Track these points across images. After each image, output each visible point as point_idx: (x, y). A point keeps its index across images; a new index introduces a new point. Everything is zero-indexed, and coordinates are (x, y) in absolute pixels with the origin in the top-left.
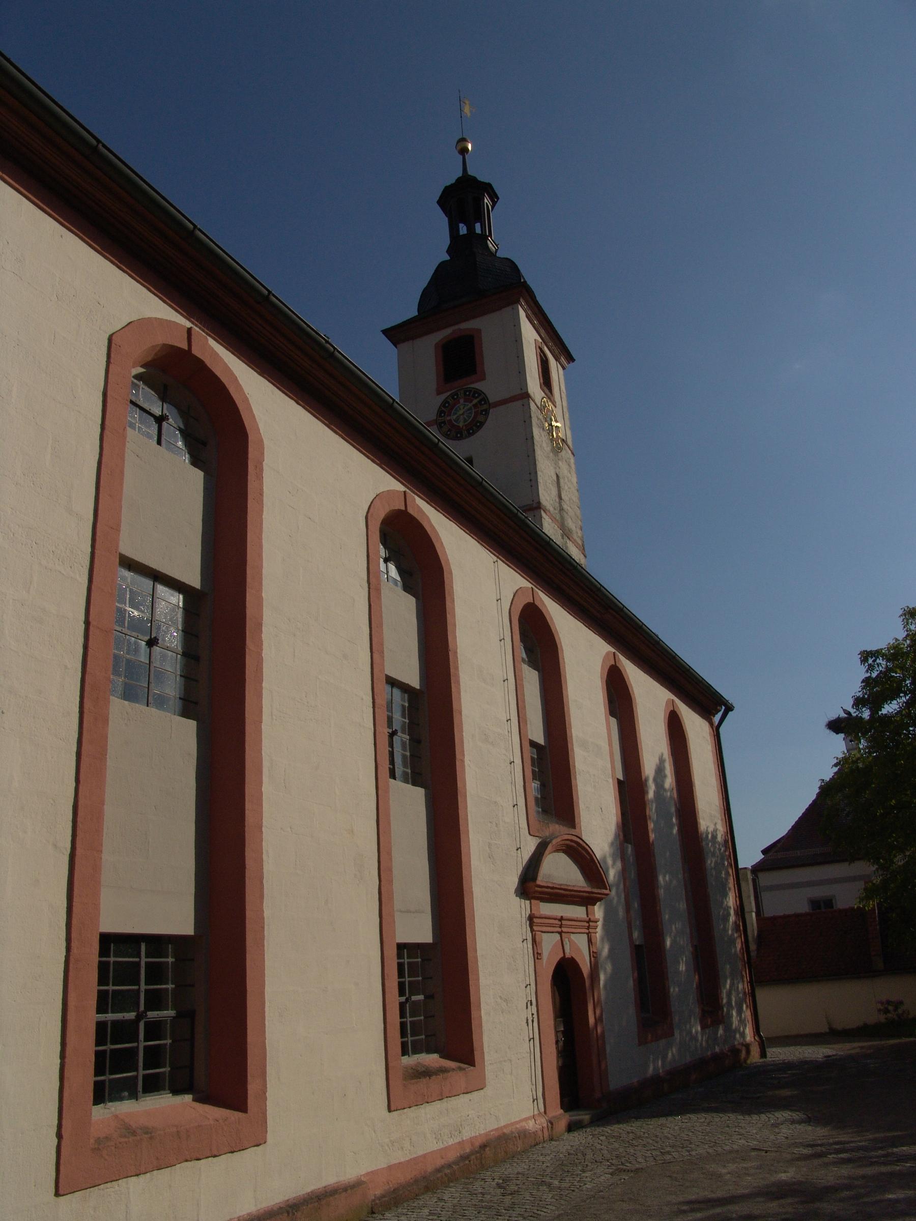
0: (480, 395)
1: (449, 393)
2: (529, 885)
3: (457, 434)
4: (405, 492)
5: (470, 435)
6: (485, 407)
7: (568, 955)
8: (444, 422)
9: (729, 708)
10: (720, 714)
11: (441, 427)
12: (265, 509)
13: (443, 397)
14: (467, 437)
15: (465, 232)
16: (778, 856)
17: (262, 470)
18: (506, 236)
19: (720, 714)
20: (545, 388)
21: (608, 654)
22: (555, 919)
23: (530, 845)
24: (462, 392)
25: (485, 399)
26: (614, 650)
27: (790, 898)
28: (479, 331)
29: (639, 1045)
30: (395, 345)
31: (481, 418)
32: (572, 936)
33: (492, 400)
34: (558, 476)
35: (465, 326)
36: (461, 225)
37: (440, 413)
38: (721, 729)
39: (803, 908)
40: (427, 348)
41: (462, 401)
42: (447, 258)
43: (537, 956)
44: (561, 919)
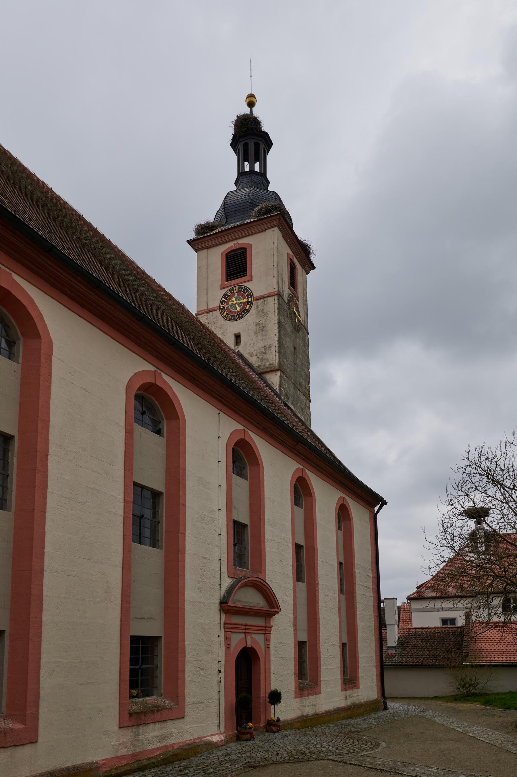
0: (248, 291)
1: (229, 288)
2: (225, 606)
3: (231, 317)
4: (155, 371)
5: (240, 318)
6: (251, 299)
7: (249, 645)
8: (224, 308)
9: (384, 503)
10: (378, 506)
11: (222, 312)
12: (52, 384)
13: (224, 291)
14: (238, 320)
15: (248, 170)
16: (422, 595)
17: (51, 360)
18: (281, 172)
19: (378, 506)
20: (292, 289)
21: (297, 469)
22: (242, 625)
23: (227, 582)
24: (237, 288)
25: (250, 295)
26: (301, 467)
27: (427, 619)
28: (251, 246)
29: (295, 698)
30: (196, 251)
31: (247, 307)
32: (253, 636)
33: (256, 294)
34: (295, 348)
35: (240, 241)
36: (246, 163)
37: (222, 302)
38: (378, 516)
39: (438, 624)
40: (216, 256)
41: (236, 294)
42: (234, 188)
43: (228, 646)
44: (246, 625)
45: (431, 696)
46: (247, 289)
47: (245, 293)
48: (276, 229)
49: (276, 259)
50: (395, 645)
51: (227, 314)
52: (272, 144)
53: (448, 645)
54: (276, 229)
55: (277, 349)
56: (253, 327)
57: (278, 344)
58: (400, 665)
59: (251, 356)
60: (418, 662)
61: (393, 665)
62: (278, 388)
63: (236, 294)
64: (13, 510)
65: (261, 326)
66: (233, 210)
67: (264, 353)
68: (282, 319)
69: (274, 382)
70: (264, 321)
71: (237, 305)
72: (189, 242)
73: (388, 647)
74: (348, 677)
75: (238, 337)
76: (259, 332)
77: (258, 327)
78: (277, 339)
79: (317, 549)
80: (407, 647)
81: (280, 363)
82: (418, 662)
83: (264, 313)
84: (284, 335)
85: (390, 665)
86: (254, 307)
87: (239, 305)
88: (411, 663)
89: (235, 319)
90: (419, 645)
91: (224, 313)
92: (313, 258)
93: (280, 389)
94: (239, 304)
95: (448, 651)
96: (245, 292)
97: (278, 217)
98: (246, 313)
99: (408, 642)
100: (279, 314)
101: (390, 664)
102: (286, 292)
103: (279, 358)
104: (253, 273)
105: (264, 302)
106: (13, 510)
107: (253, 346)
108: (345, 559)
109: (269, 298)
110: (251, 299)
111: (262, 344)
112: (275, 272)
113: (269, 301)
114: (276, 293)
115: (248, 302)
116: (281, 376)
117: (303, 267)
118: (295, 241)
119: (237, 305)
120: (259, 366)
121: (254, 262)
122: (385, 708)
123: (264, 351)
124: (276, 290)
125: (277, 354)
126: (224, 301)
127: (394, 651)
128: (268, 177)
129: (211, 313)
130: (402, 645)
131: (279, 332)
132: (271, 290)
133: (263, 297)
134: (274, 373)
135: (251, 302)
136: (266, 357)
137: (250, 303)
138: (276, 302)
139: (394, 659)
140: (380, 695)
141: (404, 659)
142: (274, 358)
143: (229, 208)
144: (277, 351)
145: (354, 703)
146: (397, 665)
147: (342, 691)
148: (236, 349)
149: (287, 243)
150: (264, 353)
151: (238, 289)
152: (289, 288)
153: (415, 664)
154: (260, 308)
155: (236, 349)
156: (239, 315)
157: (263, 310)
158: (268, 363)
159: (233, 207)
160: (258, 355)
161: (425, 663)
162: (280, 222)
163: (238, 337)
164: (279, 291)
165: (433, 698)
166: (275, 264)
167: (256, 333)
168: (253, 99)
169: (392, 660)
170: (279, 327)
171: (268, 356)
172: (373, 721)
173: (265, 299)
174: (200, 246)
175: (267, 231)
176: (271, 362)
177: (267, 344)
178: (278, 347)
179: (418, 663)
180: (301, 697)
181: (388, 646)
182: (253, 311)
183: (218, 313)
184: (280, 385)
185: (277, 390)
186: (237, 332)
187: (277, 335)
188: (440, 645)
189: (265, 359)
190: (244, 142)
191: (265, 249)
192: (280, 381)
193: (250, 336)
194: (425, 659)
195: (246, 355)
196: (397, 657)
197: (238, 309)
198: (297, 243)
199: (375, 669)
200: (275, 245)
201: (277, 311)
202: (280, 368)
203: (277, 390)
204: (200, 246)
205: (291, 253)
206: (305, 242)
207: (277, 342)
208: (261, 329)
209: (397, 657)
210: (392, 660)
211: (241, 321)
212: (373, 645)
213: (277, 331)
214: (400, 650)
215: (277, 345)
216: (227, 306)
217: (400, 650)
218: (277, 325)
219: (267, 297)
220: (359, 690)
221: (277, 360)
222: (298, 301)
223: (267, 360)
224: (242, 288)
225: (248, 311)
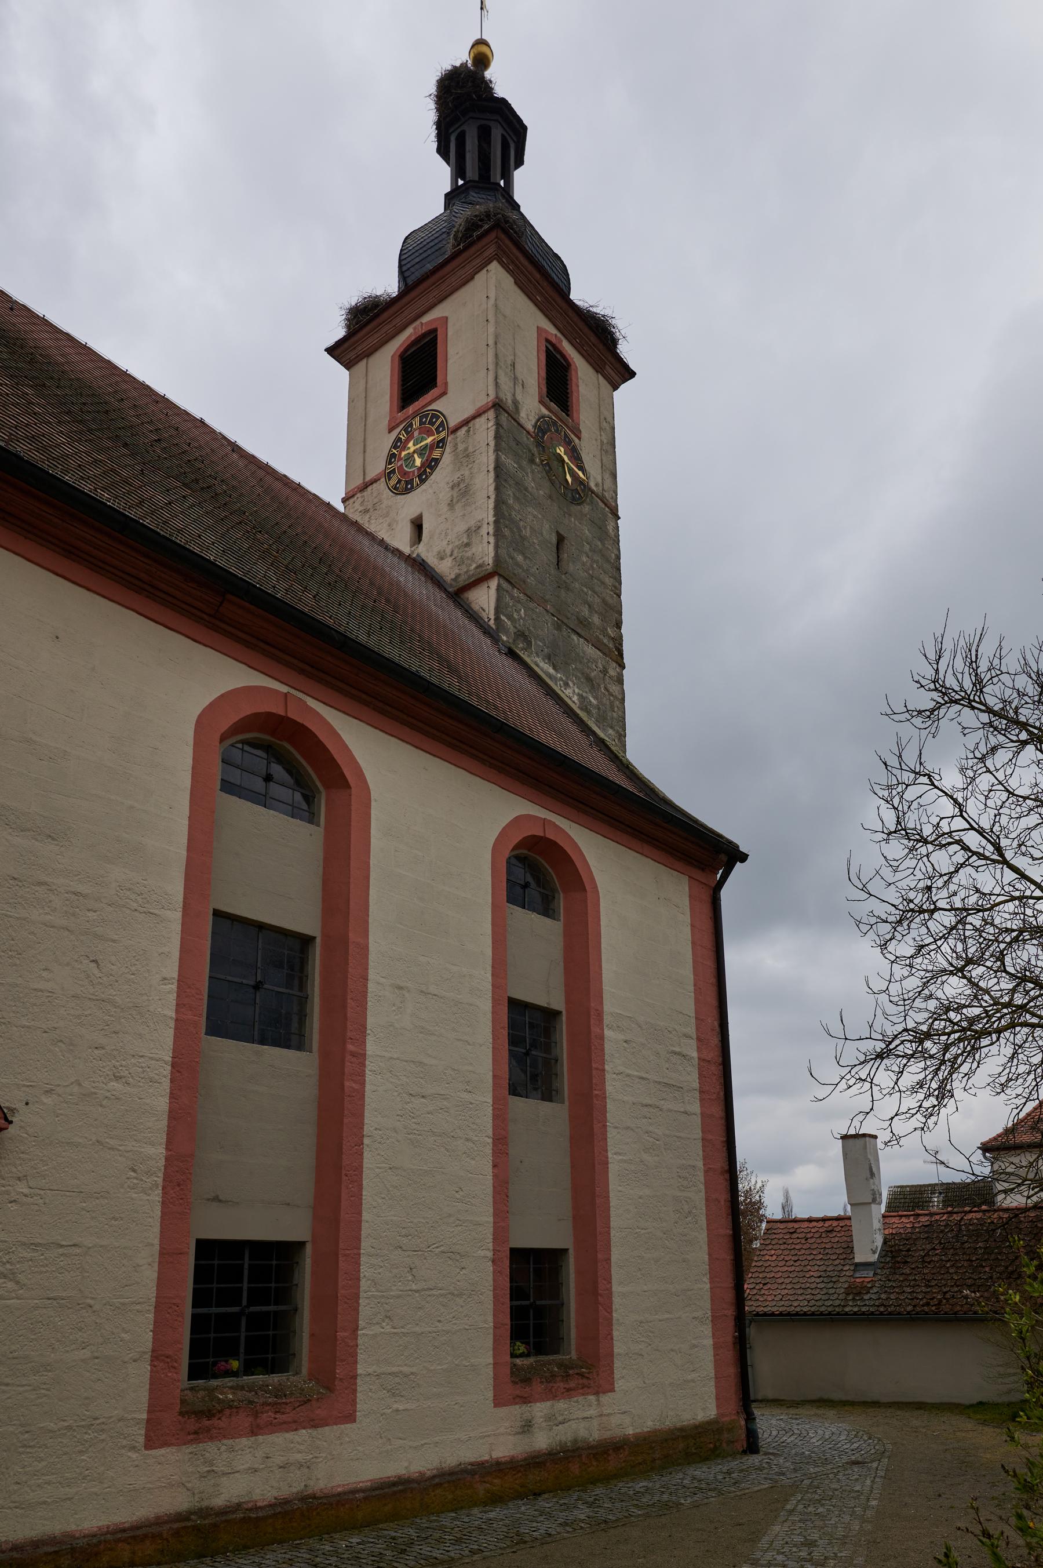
0: (438, 417)
5: (423, 481)
6: (443, 434)
30: (348, 366)
31: (436, 454)
35: (426, 319)
45: (967, 1402)
46: (436, 415)
47: (433, 424)
48: (494, 266)
49: (491, 329)
50: (874, 1258)
51: (399, 481)
52: (525, 128)
53: (1011, 1257)
54: (494, 266)
55: (491, 530)
56: (445, 495)
57: (495, 516)
58: (881, 1313)
59: (442, 559)
60: (928, 1304)
61: (863, 1313)
62: (492, 617)
63: (416, 434)
64: (315, 1046)
65: (462, 486)
66: (417, 260)
67: (467, 545)
68: (508, 462)
69: (485, 607)
70: (467, 473)
71: (416, 456)
72: (330, 351)
73: (857, 1265)
74: (574, 1355)
75: (418, 526)
76: (458, 501)
77: (456, 490)
78: (491, 505)
79: (364, 949)
80: (906, 1262)
81: (497, 558)
82: (928, 1304)
83: (468, 456)
84: (516, 498)
85: (855, 1313)
86: (448, 449)
87: (421, 455)
88: (909, 1308)
89: (412, 487)
90: (936, 1259)
91: (393, 482)
92: (624, 350)
93: (497, 619)
94: (421, 452)
95: (1012, 1272)
96: (434, 421)
97: (493, 235)
98: (433, 469)
99: (909, 1250)
100: (497, 449)
101: (856, 1309)
102: (531, 407)
103: (497, 547)
104: (450, 379)
105: (468, 431)
106: (315, 1046)
107: (446, 535)
108: (568, 1001)
109: (477, 420)
110: (443, 434)
111: (462, 527)
112: (491, 358)
113: (477, 426)
114: (490, 404)
115: (439, 442)
116: (499, 588)
117: (598, 367)
118: (571, 313)
119: (416, 456)
120: (458, 576)
121: (451, 351)
122: (752, 1446)
123: (466, 541)
124: (492, 396)
125: (492, 540)
126: (393, 455)
127: (871, 1274)
128: (517, 197)
129: (369, 488)
130: (893, 1257)
131: (497, 489)
132: (483, 401)
133: (466, 422)
134: (484, 585)
135: (443, 440)
136: (469, 554)
137: (441, 444)
138: (491, 424)
139: (866, 1297)
140: (733, 1405)
141: (892, 1296)
142: (485, 552)
143: (409, 259)
144: (491, 532)
145: (575, 1441)
146: (872, 1313)
147: (498, 1403)
148: (413, 552)
149: (536, 305)
150: (467, 545)
151: (420, 420)
152: (541, 402)
153: (918, 1309)
154: (461, 447)
155: (413, 552)
156: (420, 476)
157: (466, 449)
158: (474, 566)
159: (417, 254)
160: (455, 554)
161: (946, 1308)
162: (499, 247)
163: (418, 526)
164: (497, 397)
165: (972, 1406)
166: (491, 342)
167: (451, 505)
168: (483, 49)
169: (862, 1299)
170: (497, 477)
171: (474, 550)
172: (355, 1540)
173: (471, 424)
174: (352, 355)
175: (476, 277)
176: (481, 562)
177: (472, 523)
178: (495, 522)
179: (926, 1308)
180: (198, 1436)
181: (857, 1260)
182: (447, 459)
183: (381, 485)
184: (498, 610)
185: (492, 623)
186: (413, 514)
187: (493, 497)
188: (993, 1256)
189: (468, 558)
190: (459, 130)
191: (484, 327)
192: (499, 600)
193: (440, 516)
194: (948, 1296)
195: (431, 560)
196: (875, 1290)
197: (418, 462)
198: (576, 318)
199: (707, 1330)
200: (492, 301)
201: (492, 443)
202: (497, 571)
203: (492, 623)
204: (352, 355)
205: (553, 330)
206: (594, 310)
207: (491, 512)
208: (462, 491)
209: (875, 1290)
210: (862, 1299)
211: (423, 487)
212: (701, 1255)
213: (492, 488)
214: (887, 1271)
215: (491, 519)
216: (399, 463)
217: (887, 1271)
218: (492, 474)
219: (474, 417)
220: (605, 1399)
221: (492, 554)
222: (579, 439)
223: (472, 559)
224: (426, 416)
225: (437, 461)
